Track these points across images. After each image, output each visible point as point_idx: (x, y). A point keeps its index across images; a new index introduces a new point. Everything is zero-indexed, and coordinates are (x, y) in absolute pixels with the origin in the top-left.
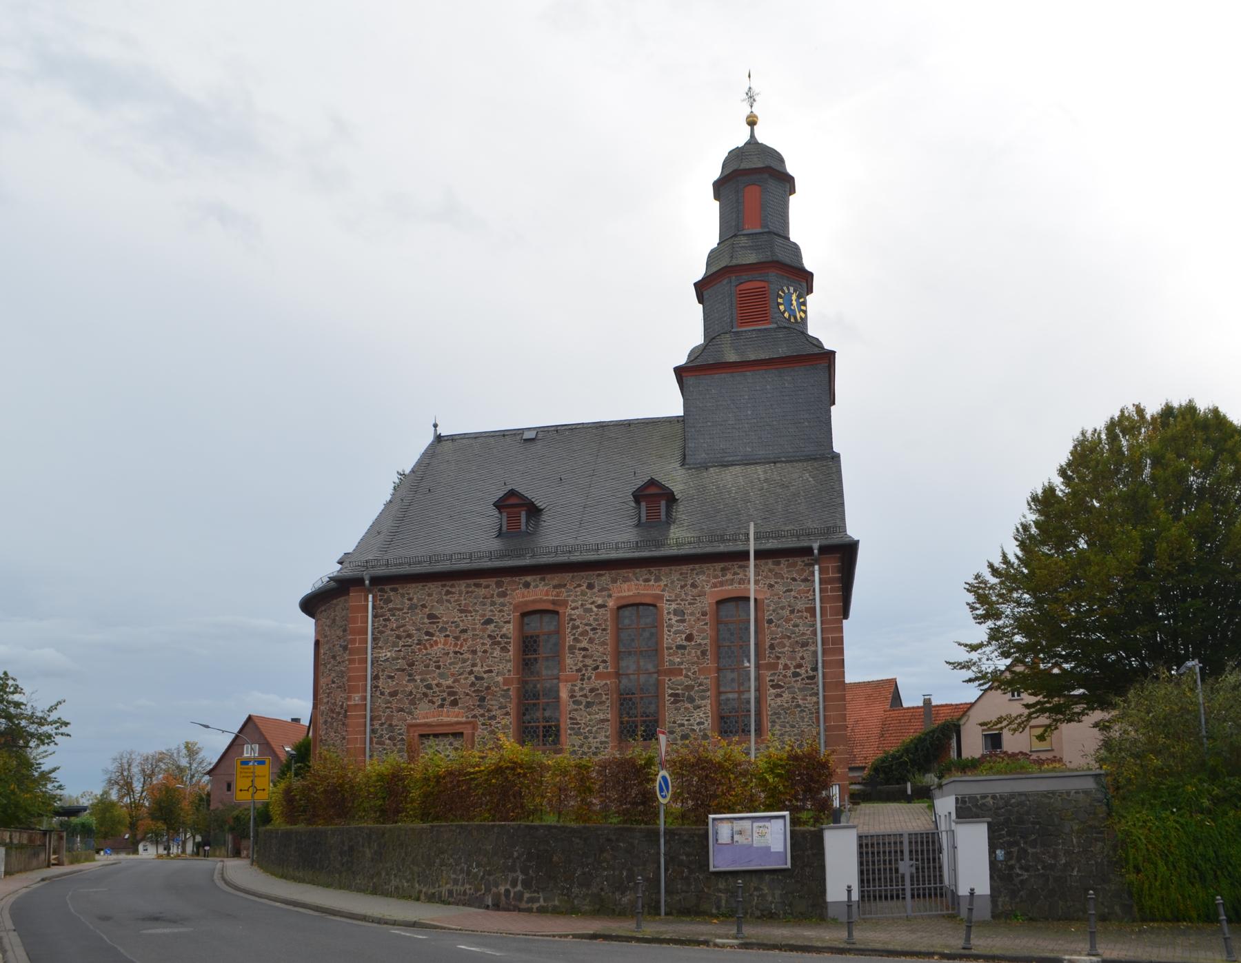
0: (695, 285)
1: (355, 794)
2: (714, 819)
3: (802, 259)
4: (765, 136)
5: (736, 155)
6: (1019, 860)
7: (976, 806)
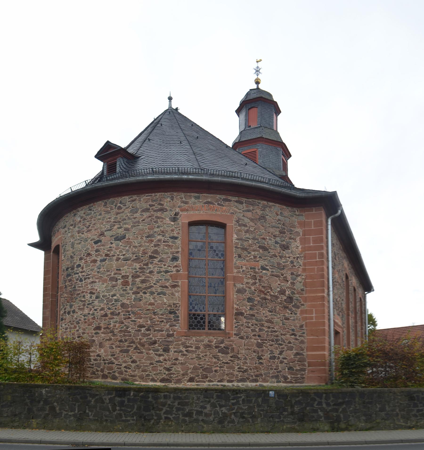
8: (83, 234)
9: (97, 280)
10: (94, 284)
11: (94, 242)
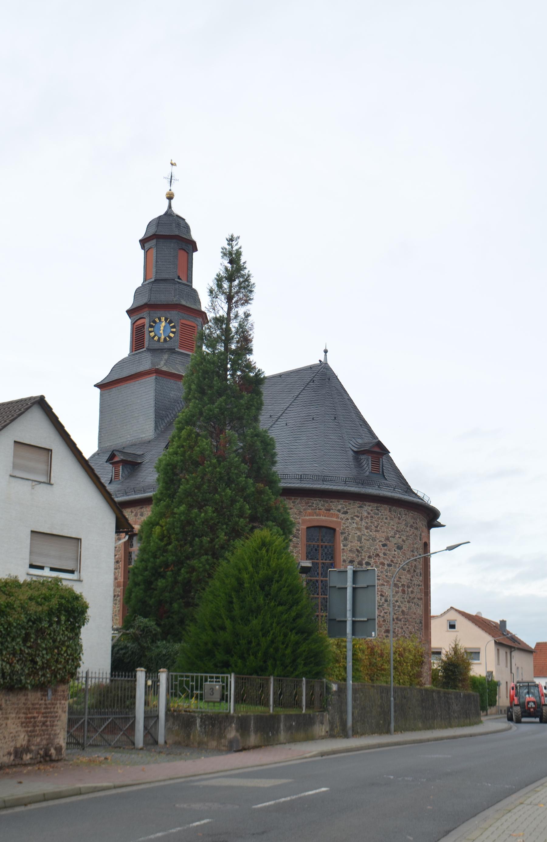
3: (198, 295)
5: (159, 222)
8: (371, 531)
9: (385, 584)
10: (383, 587)
11: (382, 544)
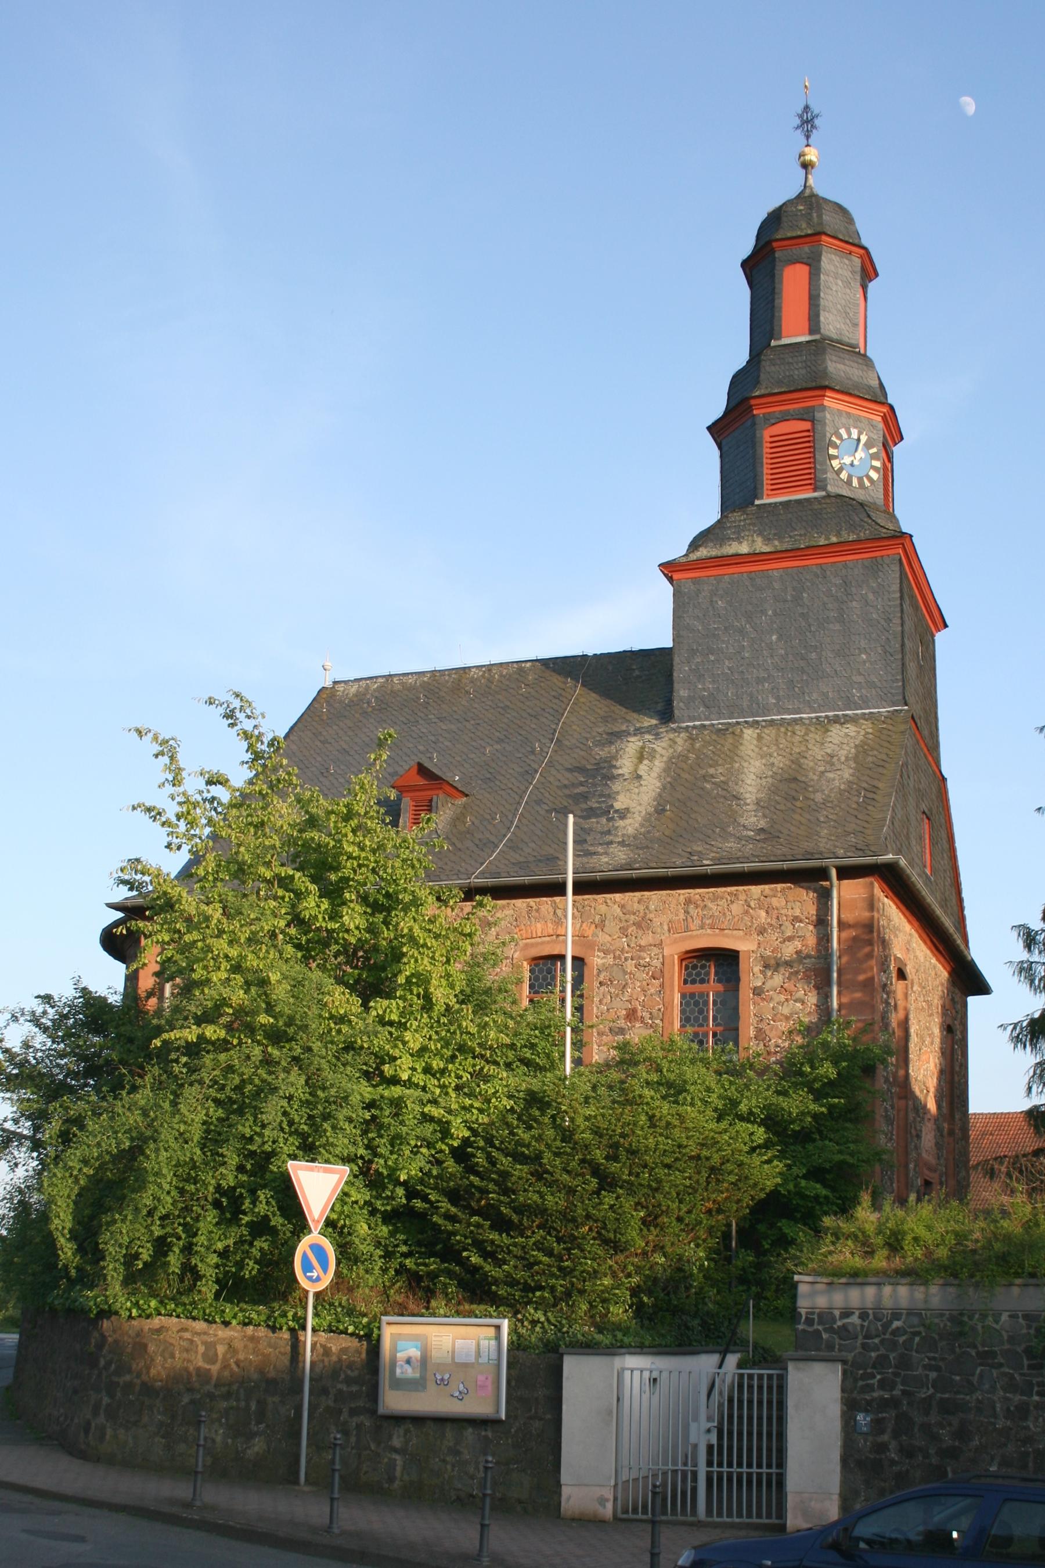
0: (709, 428)
1: (356, 1264)
2: (498, 1328)
4: (822, 186)
6: (896, 1435)
7: (831, 1330)
